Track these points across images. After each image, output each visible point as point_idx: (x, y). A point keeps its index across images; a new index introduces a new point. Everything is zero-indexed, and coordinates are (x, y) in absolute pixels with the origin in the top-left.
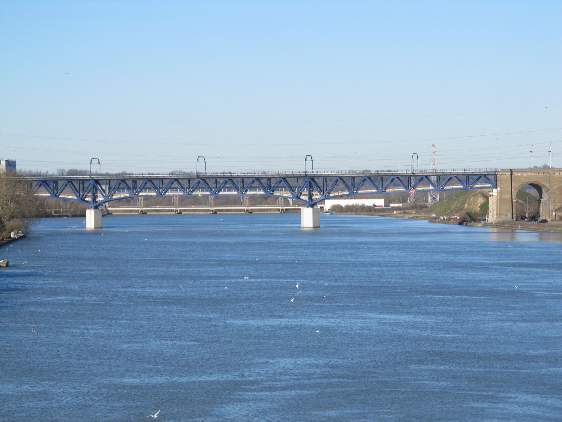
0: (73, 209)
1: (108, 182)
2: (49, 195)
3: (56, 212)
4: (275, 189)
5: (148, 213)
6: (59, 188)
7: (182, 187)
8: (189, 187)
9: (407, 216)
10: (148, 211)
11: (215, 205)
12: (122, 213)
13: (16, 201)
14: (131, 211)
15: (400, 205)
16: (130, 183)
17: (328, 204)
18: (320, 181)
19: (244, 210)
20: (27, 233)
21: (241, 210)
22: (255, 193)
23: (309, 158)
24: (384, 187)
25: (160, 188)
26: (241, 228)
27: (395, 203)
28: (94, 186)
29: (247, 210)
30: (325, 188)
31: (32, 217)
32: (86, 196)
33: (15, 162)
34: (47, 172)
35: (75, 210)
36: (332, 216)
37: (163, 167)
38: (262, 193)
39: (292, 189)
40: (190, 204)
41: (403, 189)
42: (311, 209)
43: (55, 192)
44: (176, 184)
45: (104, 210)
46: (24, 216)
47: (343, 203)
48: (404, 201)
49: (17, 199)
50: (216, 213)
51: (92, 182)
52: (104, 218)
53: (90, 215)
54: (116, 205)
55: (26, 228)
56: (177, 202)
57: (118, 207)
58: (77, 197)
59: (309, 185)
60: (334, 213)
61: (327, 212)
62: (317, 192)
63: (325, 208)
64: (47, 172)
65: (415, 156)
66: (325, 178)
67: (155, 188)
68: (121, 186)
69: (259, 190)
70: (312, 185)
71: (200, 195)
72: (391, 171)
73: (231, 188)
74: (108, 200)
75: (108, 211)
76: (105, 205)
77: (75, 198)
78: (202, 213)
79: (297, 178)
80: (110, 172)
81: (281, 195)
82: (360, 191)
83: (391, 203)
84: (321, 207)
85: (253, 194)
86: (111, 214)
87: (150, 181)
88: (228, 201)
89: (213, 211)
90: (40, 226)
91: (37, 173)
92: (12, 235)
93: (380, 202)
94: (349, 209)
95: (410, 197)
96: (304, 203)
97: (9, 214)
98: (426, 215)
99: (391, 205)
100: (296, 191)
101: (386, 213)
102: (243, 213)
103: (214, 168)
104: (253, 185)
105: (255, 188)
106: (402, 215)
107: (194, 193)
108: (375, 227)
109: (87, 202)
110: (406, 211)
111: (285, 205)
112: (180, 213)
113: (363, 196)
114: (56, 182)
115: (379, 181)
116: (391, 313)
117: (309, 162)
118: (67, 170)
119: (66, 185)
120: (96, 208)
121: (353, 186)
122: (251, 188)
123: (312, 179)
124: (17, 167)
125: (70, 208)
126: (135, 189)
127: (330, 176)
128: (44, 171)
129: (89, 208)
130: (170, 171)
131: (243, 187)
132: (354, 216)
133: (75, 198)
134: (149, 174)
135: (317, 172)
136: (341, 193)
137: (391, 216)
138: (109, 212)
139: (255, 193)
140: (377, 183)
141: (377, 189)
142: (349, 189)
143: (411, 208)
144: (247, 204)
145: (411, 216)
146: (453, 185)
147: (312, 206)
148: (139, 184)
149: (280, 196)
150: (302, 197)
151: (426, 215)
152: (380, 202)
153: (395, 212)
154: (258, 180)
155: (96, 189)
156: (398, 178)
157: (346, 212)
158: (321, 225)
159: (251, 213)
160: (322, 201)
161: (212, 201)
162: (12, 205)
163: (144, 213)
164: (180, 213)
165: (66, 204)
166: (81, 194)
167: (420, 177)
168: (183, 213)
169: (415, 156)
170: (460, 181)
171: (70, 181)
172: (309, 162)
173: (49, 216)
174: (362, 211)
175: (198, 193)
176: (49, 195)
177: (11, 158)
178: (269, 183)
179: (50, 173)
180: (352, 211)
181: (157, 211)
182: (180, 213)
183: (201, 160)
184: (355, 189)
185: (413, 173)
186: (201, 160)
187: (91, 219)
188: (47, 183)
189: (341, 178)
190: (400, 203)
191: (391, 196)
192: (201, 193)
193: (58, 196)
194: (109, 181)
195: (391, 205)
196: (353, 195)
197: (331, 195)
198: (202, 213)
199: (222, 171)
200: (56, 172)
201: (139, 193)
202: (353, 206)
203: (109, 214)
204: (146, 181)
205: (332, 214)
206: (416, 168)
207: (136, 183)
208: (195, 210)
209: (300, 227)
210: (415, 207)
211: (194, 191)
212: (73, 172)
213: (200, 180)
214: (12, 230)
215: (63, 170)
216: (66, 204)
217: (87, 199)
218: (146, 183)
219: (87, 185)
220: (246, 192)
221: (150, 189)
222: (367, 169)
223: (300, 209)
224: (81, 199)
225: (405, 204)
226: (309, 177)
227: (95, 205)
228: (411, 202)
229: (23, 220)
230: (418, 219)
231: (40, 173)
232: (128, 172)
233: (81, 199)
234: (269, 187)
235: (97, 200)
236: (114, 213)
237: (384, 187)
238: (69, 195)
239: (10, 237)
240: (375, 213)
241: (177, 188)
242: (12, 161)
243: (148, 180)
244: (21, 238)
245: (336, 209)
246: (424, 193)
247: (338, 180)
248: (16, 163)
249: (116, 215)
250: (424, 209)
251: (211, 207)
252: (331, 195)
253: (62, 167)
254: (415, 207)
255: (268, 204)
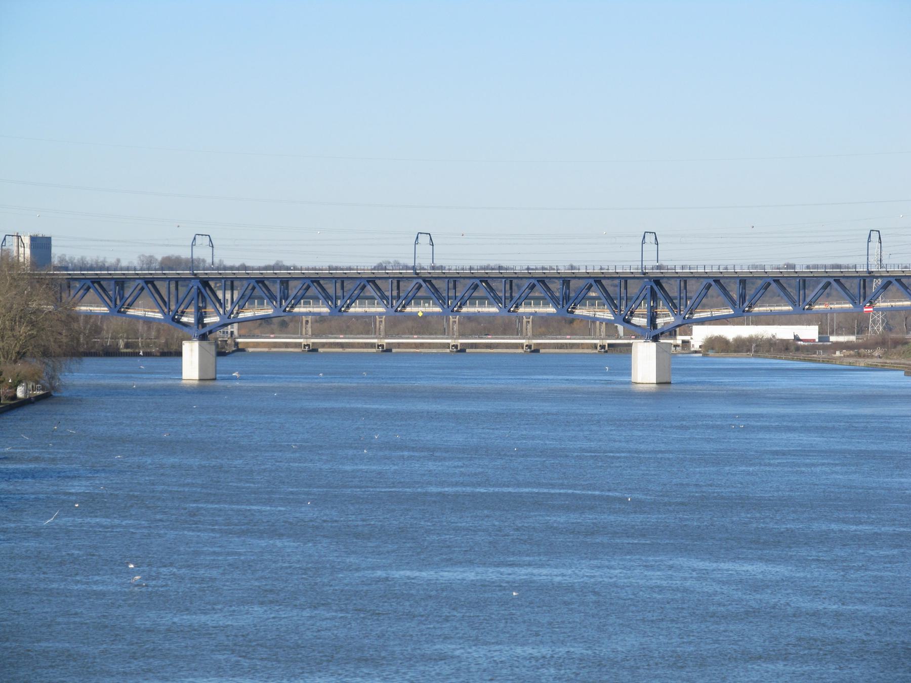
0: (162, 341)
1: (229, 283)
2: (105, 310)
3: (127, 346)
4: (581, 299)
5: (320, 350)
6: (127, 295)
7: (383, 297)
8: (399, 297)
9: (862, 363)
10: (323, 345)
11: (462, 335)
12: (266, 350)
13: (32, 324)
14: (287, 345)
15: (852, 338)
16: (276, 289)
17: (699, 335)
18: (672, 289)
19: (521, 346)
20: (53, 388)
21: (516, 346)
22: (537, 310)
23: (650, 238)
24: (808, 300)
25: (337, 298)
26: (504, 382)
27: (842, 335)
28: (199, 293)
29: (529, 346)
30: (683, 301)
31: (65, 355)
32: (183, 312)
33: (49, 239)
34: (118, 260)
35: (166, 343)
36: (706, 359)
37: (359, 255)
38: (551, 310)
39: (611, 301)
40: (411, 332)
41: (849, 306)
42: (654, 344)
43: (119, 306)
44: (370, 290)
45: (229, 342)
46: (46, 353)
47: (731, 332)
48: (860, 331)
49: (33, 318)
50: (463, 351)
51: (196, 284)
52: (222, 360)
53: (191, 352)
54: (257, 332)
55: (52, 378)
56: (382, 327)
57: (258, 337)
58: (164, 314)
59: (648, 296)
60: (711, 353)
61: (696, 352)
62: (666, 311)
63: (692, 342)
64: (118, 260)
65: (875, 236)
66: (684, 280)
67: (328, 297)
68: (309, 293)
69: (546, 304)
70: (661, 295)
71: (420, 314)
72: (839, 267)
73: (487, 298)
74: (229, 321)
75: (237, 344)
76: (232, 333)
77: (159, 316)
78: (434, 351)
79: (624, 280)
80: (249, 263)
81: (591, 314)
82: (756, 309)
83: (832, 333)
84: (684, 342)
85: (474, 313)
86: (243, 350)
87: (316, 284)
88: (484, 326)
89: (456, 346)
90: (81, 376)
91: (97, 262)
92: (20, 393)
93: (810, 332)
94: (742, 346)
95: (874, 321)
96: (639, 332)
97: (17, 349)
98: (903, 361)
99: (833, 339)
100: (623, 308)
101: (821, 355)
102: (520, 351)
103: (458, 254)
104: (419, 294)
105: (537, 301)
106: (851, 360)
107: (408, 309)
108: (783, 383)
109: (186, 325)
110: (862, 351)
111: (609, 336)
112: (389, 350)
113: (760, 320)
114: (121, 283)
115: (795, 289)
116: (751, 559)
117: (650, 247)
118: (159, 257)
119: (142, 289)
120: (203, 338)
121: (743, 297)
122: (527, 299)
123: (657, 282)
124: (54, 250)
125: (157, 337)
126: (286, 299)
127: (698, 277)
128: (110, 260)
129: (189, 339)
130: (374, 262)
131: (511, 297)
132: (753, 360)
133: (159, 316)
134: (330, 268)
135: (683, 268)
136: (717, 313)
137: (828, 362)
138: (240, 346)
139: (537, 310)
140: (793, 292)
141: (793, 303)
142: (733, 303)
143: (874, 345)
144: (530, 334)
145: (870, 361)
146: (893, 299)
147: (655, 339)
148: (294, 289)
149: (588, 317)
150: (635, 320)
151: (903, 361)
152: (810, 332)
153: (838, 353)
154: (540, 284)
155: (204, 300)
156: (837, 281)
157: (735, 351)
158: (674, 379)
159: (536, 351)
160: (686, 325)
161: (456, 327)
162: (23, 330)
163: (313, 350)
164: (388, 350)
165: (149, 328)
166: (173, 307)
167: (886, 280)
168: (394, 350)
169: (875, 236)
170: (437, 296)
171: (150, 281)
172: (650, 247)
173: (111, 352)
174: (768, 351)
175: (419, 310)
176: (105, 310)
177: (42, 232)
178: (566, 290)
179: (124, 263)
180: (749, 350)
181: (341, 345)
182: (389, 350)
183: (424, 239)
184: (747, 303)
185: (645, 274)
186: (424, 239)
187: (192, 360)
188: (114, 286)
189: (717, 281)
190: (853, 334)
191: (832, 320)
192: (423, 309)
193: (124, 312)
194: (231, 283)
195: (833, 339)
196: (741, 316)
197: (696, 316)
198: (434, 351)
199: (484, 263)
200: (136, 263)
201: (292, 307)
202: (751, 340)
203: (239, 350)
204: (308, 282)
205: (705, 355)
206: (874, 260)
207: (287, 288)
208: (421, 345)
209: (630, 383)
210: (882, 343)
211: (408, 304)
212: (170, 263)
213: (421, 281)
214: (19, 383)
215: (151, 259)
216: (149, 328)
217: (184, 319)
218: (308, 287)
219: (191, 287)
220: (517, 307)
221: (316, 299)
222: (791, 262)
223: (630, 345)
224: (173, 319)
225: (860, 336)
226: (650, 278)
227: (202, 331)
228: (875, 332)
229: (46, 360)
230: (883, 368)
231: (104, 262)
232: (287, 263)
233: (173, 319)
234: (566, 298)
235: (206, 320)
236: (251, 350)
237: (808, 300)
238: (145, 311)
239: (15, 397)
240: (798, 354)
241: (373, 298)
242: (43, 238)
243: (313, 282)
244: (39, 398)
245: (715, 345)
246: (903, 313)
247: (710, 286)
248: (53, 243)
249: (253, 352)
250: (899, 347)
251: (452, 338)
252: (696, 316)
253: (148, 251)
254: (882, 343)
255: (573, 334)
